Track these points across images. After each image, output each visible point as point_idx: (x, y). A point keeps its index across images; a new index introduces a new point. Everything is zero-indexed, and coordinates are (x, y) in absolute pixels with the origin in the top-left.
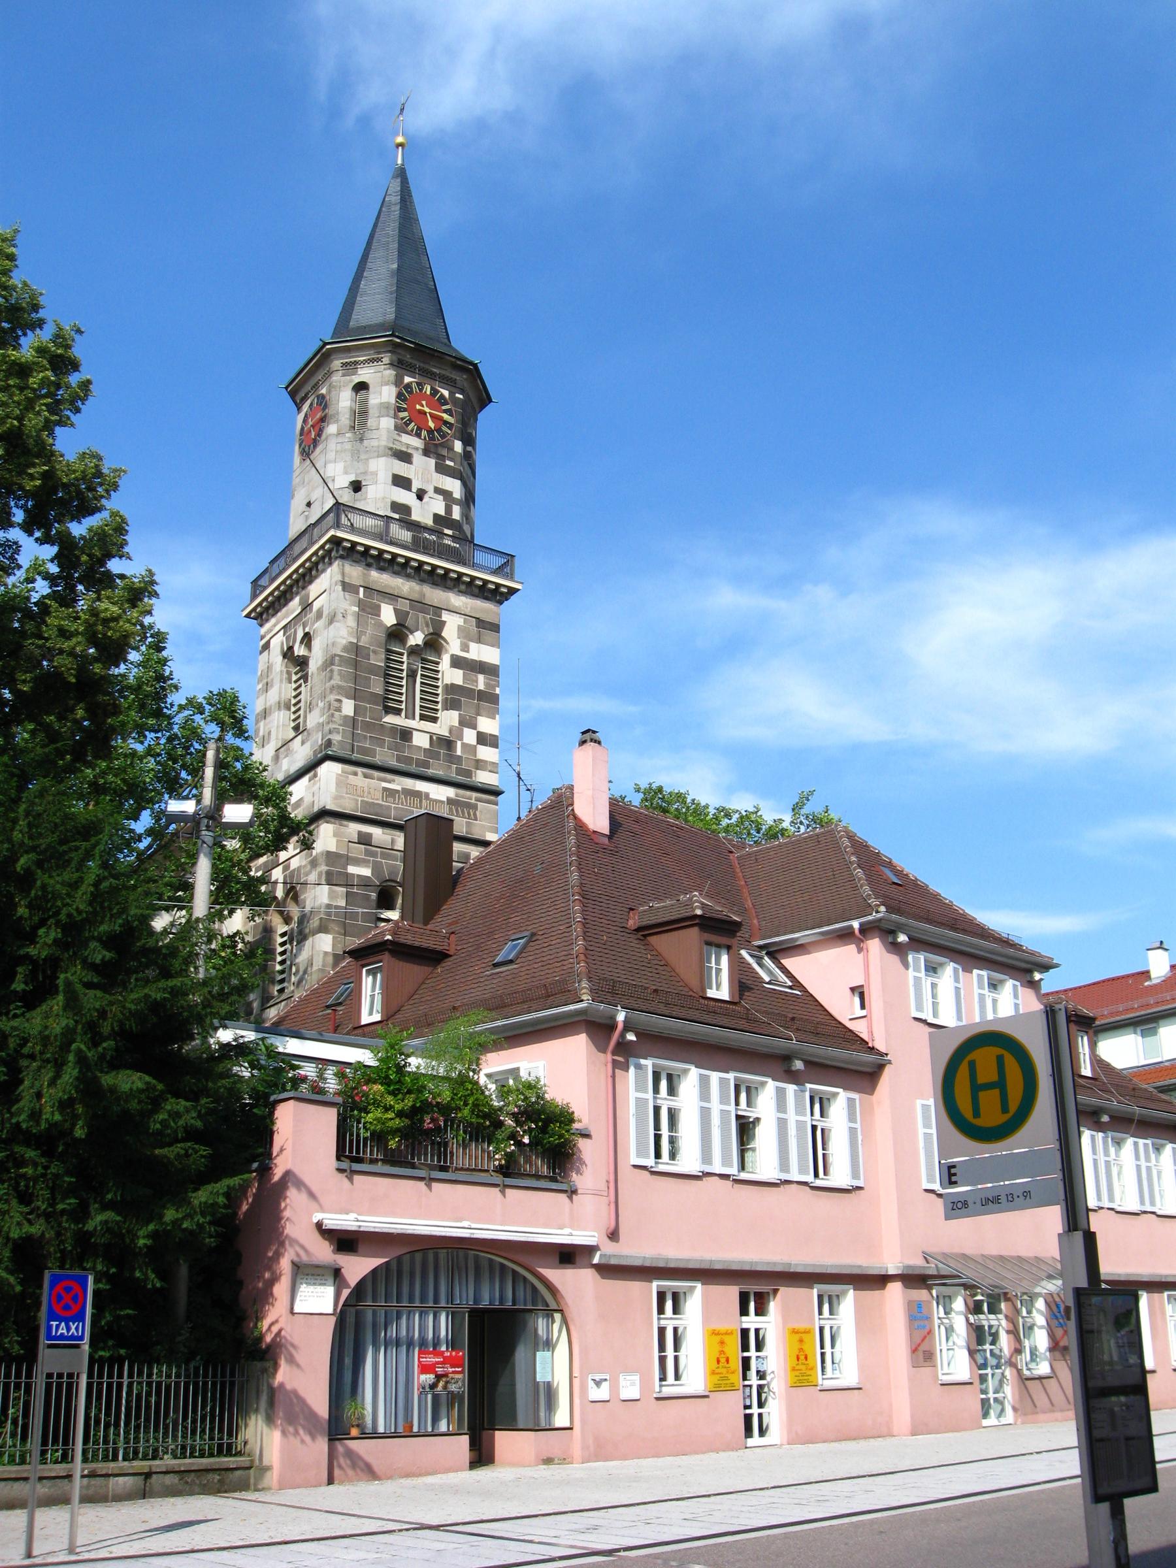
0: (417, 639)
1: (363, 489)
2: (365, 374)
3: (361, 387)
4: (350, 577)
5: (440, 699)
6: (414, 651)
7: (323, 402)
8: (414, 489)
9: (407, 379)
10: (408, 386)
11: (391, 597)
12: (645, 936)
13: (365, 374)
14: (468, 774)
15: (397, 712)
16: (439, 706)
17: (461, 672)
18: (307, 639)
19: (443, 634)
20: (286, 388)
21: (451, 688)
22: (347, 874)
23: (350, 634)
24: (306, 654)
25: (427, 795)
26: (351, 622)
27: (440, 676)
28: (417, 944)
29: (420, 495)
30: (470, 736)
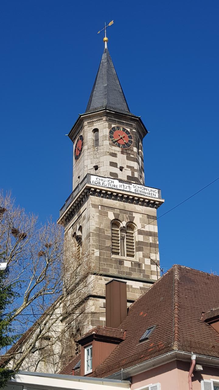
0: (123, 224)
1: (99, 168)
2: (96, 125)
3: (96, 130)
4: (95, 202)
5: (134, 247)
6: (122, 230)
7: (82, 138)
8: (119, 167)
9: (113, 126)
10: (114, 128)
11: (112, 208)
12: (210, 324)
13: (96, 125)
14: (148, 276)
15: (118, 253)
16: (135, 250)
17: (142, 236)
18: (80, 228)
19: (134, 222)
20: (68, 135)
21: (139, 243)
22: (99, 321)
23: (96, 224)
24: (81, 234)
25: (131, 286)
26: (96, 219)
27: (134, 238)
28: (108, 335)
29: (121, 169)
30: (147, 262)
